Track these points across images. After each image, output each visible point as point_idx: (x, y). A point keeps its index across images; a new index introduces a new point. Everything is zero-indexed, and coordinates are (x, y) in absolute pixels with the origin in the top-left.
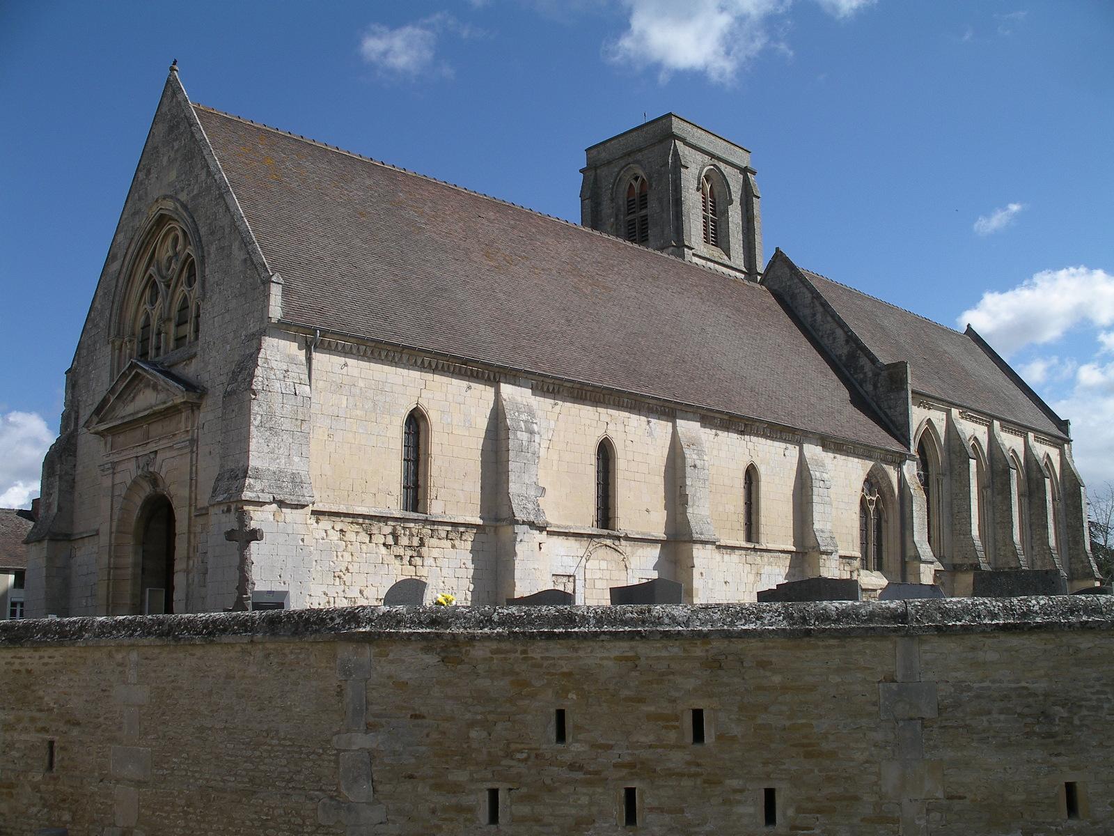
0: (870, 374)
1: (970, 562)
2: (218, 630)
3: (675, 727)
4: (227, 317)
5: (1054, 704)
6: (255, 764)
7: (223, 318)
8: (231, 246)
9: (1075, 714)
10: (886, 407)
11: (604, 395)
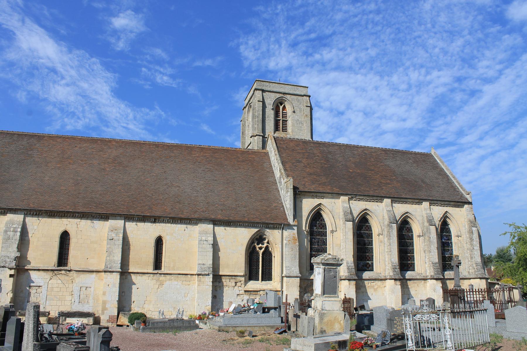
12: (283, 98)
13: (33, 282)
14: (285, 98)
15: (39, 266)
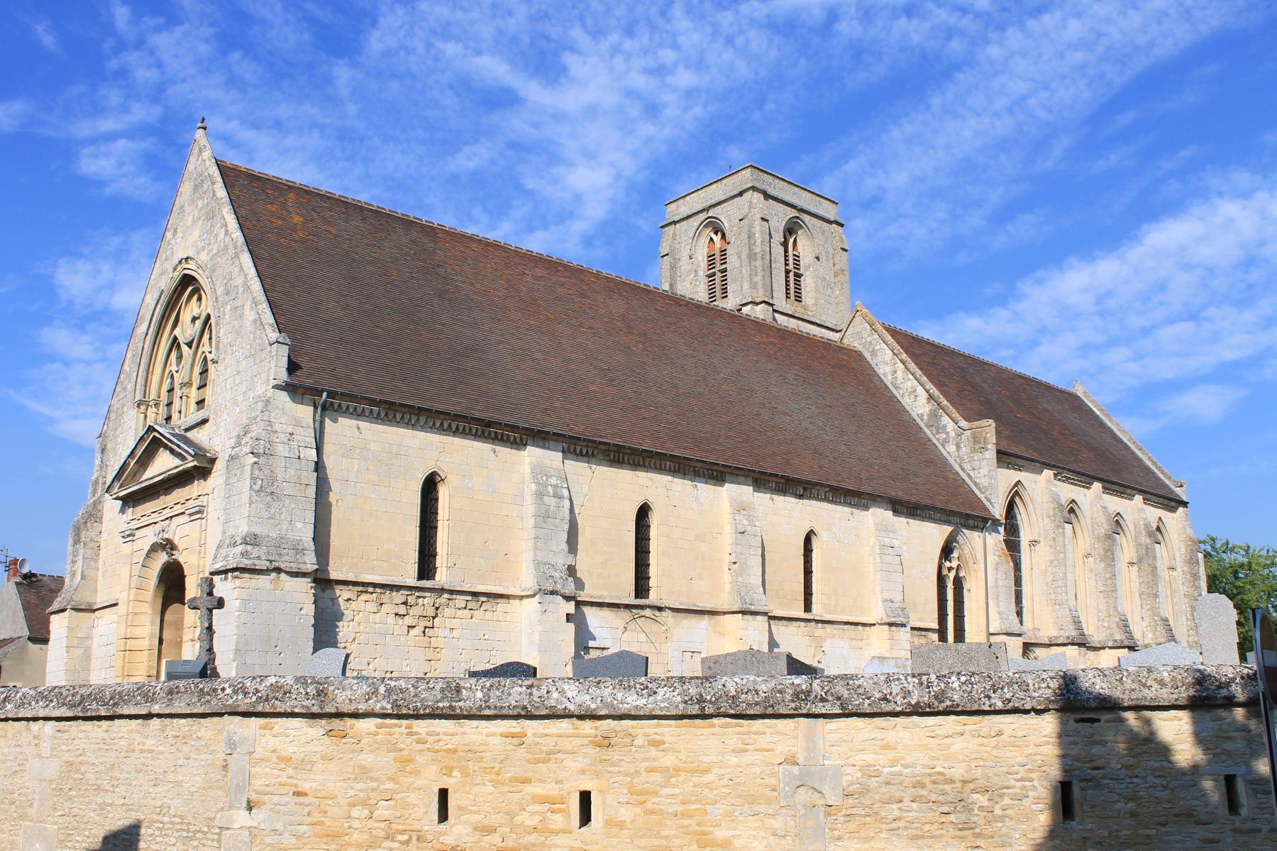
0: (952, 434)
1: (1067, 634)
2: (123, 701)
3: (560, 811)
4: (238, 379)
5: (974, 791)
6: (148, 843)
7: (234, 380)
8: (243, 306)
9: (997, 803)
10: (969, 469)
11: (644, 458)
12: (798, 221)
13: (594, 639)
14: (803, 222)
15: (601, 593)
